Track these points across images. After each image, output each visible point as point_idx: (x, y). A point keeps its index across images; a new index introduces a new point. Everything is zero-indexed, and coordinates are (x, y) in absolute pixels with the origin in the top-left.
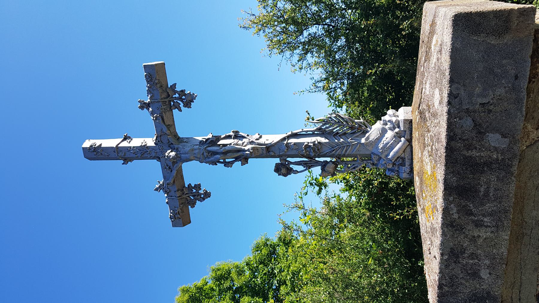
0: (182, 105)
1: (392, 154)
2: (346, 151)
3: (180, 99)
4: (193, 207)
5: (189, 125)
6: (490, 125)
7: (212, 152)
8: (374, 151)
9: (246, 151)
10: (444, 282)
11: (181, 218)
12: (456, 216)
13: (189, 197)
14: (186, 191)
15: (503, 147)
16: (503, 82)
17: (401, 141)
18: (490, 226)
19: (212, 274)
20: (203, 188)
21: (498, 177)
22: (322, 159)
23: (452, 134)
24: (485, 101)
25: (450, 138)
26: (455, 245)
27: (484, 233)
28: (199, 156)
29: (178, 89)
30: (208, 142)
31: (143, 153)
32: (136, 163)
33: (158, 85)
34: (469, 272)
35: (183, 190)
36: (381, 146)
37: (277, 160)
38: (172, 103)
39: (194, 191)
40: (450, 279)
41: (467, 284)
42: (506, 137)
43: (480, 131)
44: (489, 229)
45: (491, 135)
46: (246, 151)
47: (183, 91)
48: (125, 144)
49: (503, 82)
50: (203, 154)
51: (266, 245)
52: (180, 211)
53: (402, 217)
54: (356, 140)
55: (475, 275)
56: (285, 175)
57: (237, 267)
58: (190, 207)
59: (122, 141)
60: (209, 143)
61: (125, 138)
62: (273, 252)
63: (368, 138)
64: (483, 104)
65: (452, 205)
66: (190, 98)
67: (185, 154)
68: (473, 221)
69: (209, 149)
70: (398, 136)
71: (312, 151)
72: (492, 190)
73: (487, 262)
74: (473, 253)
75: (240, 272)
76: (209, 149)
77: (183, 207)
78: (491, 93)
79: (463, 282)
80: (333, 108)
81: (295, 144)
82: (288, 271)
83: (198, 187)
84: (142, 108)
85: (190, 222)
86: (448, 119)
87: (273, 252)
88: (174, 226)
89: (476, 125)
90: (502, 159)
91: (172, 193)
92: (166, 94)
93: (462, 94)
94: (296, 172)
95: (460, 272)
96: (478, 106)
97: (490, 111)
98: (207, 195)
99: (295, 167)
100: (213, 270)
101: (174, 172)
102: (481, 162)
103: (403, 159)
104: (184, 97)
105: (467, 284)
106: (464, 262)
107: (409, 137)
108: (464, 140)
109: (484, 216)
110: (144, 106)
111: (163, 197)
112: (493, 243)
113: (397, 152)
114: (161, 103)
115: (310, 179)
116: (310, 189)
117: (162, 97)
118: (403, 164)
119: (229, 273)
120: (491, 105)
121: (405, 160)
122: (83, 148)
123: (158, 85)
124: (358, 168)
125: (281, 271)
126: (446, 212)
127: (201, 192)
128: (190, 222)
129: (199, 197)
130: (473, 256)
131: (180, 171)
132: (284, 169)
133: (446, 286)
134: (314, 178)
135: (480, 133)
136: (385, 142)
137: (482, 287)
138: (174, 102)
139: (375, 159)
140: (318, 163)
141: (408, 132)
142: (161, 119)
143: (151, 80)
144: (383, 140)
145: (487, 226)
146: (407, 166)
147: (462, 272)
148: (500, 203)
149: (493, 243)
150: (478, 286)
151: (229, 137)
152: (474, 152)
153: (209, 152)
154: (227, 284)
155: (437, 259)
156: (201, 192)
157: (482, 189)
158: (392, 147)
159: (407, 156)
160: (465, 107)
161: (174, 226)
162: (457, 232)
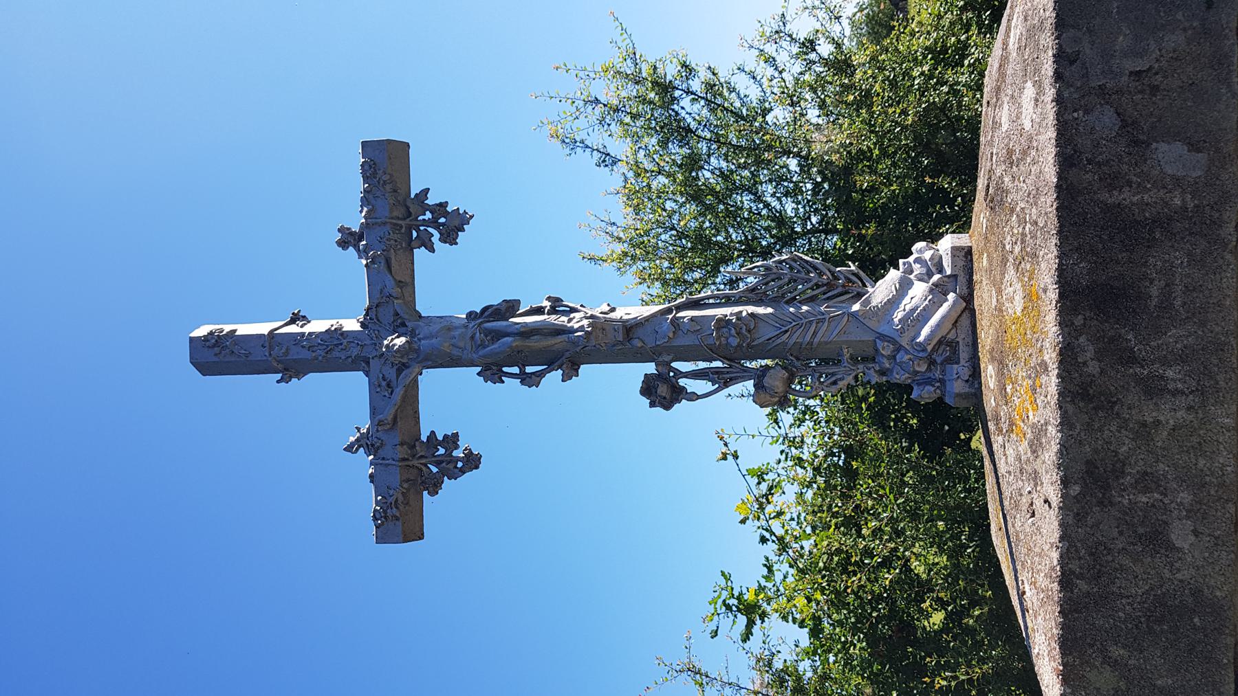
0: (436, 235)
1: (925, 332)
2: (815, 333)
3: (434, 223)
4: (433, 493)
5: (446, 285)
6: (1159, 121)
7: (517, 346)
8: (884, 329)
9: (577, 330)
10: (1074, 566)
11: (399, 520)
12: (1093, 368)
13: (425, 465)
14: (420, 451)
15: (1194, 175)
16: (1179, 16)
17: (947, 300)
18: (1183, 393)
20: (463, 444)
21: (1189, 254)
22: (754, 365)
23: (1069, 150)
24: (1141, 65)
25: (1065, 159)
26: (1096, 451)
27: (1170, 413)
28: (461, 344)
29: (431, 200)
30: (486, 314)
31: (330, 353)
32: (313, 379)
33: (388, 187)
34: (1141, 530)
35: (414, 446)
36: (898, 315)
37: (650, 368)
38: (415, 234)
39: (442, 451)
40: (1092, 554)
41: (1138, 569)
42: (1199, 151)
43: (1136, 137)
44: (1181, 401)
45: (1163, 147)
46: (577, 330)
47: (443, 205)
49: (1179, 16)
50: (472, 338)
52: (401, 498)
53: (953, 684)
54: (839, 308)
55: (1155, 539)
56: (667, 407)
58: (425, 493)
59: (286, 325)
60: (490, 315)
61: (293, 321)
63: (868, 301)
64: (1137, 74)
65: (1082, 340)
66: (456, 223)
67: (431, 336)
68: (1139, 380)
70: (939, 292)
71: (733, 331)
72: (1179, 289)
73: (1185, 497)
74: (1146, 473)
77: (408, 490)
78: (1153, 46)
79: (1127, 562)
80: (783, 447)
81: (692, 319)
83: (452, 441)
84: (343, 244)
85: (421, 537)
86: (1059, 115)
88: (379, 540)
89: (1126, 124)
90: (1196, 206)
91: (387, 451)
92: (403, 210)
93: (1088, 51)
94: (694, 397)
95: (1115, 533)
96: (1125, 78)
97: (1155, 89)
98: (472, 461)
99: (691, 385)
101: (399, 392)
102: (1146, 219)
103: (953, 345)
104: (442, 220)
105: (1138, 569)
106: (1126, 502)
107: (965, 291)
108: (1099, 164)
109: (1165, 363)
110: (348, 239)
111: (363, 462)
112: (1195, 439)
113: (939, 325)
114: (388, 227)
115: (725, 594)
116: (725, 622)
117: (395, 214)
118: (953, 359)
120: (1156, 74)
121: (959, 345)
122: (191, 339)
123: (388, 187)
124: (845, 382)
126: (1068, 356)
127: (458, 453)
128: (421, 537)
129: (451, 466)
130: (1147, 481)
131: (414, 385)
132: (664, 392)
133: (1081, 576)
134: (736, 594)
135: (1136, 143)
136: (908, 308)
137: (1179, 576)
138: (418, 231)
139: (886, 349)
140: (745, 374)
141: (962, 279)
142: (383, 262)
143: (375, 174)
144: (904, 302)
145: (1176, 393)
146: (962, 362)
147: (1121, 533)
148: (1203, 324)
149: (1195, 439)
150: (1167, 574)
151: (539, 311)
152: (1126, 193)
153: (488, 332)
155: (1054, 504)
156: (458, 453)
157: (1154, 291)
159: (962, 336)
160: (1095, 83)
161: (379, 540)
162: (1101, 414)
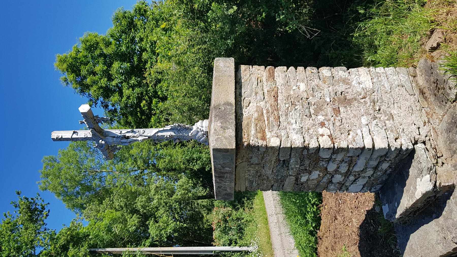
19: (81, 47)
48: (75, 136)
51: (124, 17)
57: (104, 40)
61: (74, 133)
62: (131, 25)
69: (121, 141)
75: (108, 44)
76: (121, 141)
82: (147, 40)
87: (131, 25)
100: (83, 42)
119: (97, 43)
125: (141, 40)
154: (97, 52)
158: (201, 138)
